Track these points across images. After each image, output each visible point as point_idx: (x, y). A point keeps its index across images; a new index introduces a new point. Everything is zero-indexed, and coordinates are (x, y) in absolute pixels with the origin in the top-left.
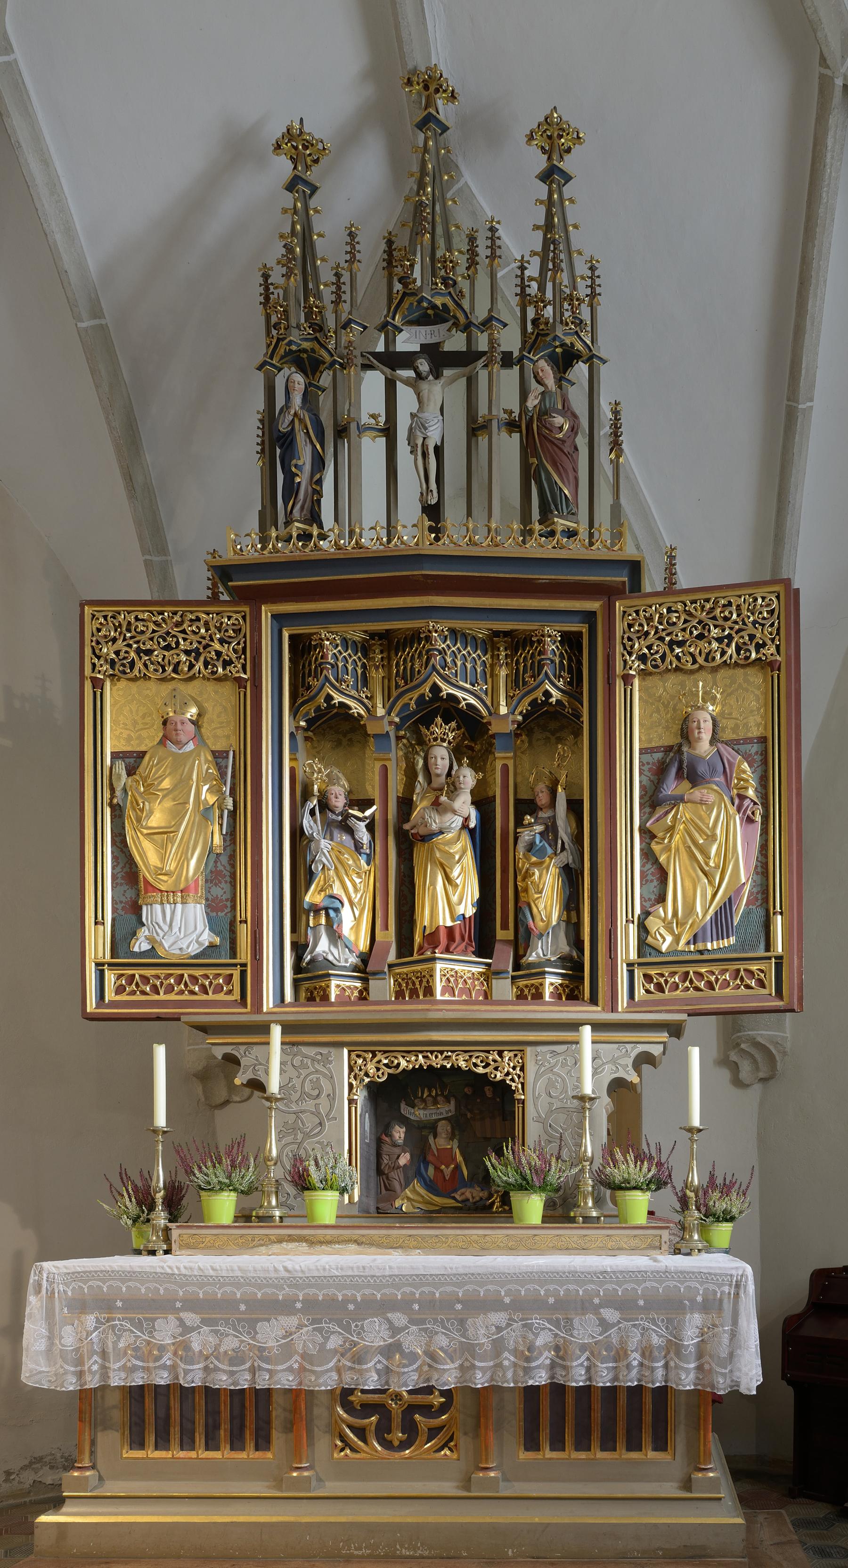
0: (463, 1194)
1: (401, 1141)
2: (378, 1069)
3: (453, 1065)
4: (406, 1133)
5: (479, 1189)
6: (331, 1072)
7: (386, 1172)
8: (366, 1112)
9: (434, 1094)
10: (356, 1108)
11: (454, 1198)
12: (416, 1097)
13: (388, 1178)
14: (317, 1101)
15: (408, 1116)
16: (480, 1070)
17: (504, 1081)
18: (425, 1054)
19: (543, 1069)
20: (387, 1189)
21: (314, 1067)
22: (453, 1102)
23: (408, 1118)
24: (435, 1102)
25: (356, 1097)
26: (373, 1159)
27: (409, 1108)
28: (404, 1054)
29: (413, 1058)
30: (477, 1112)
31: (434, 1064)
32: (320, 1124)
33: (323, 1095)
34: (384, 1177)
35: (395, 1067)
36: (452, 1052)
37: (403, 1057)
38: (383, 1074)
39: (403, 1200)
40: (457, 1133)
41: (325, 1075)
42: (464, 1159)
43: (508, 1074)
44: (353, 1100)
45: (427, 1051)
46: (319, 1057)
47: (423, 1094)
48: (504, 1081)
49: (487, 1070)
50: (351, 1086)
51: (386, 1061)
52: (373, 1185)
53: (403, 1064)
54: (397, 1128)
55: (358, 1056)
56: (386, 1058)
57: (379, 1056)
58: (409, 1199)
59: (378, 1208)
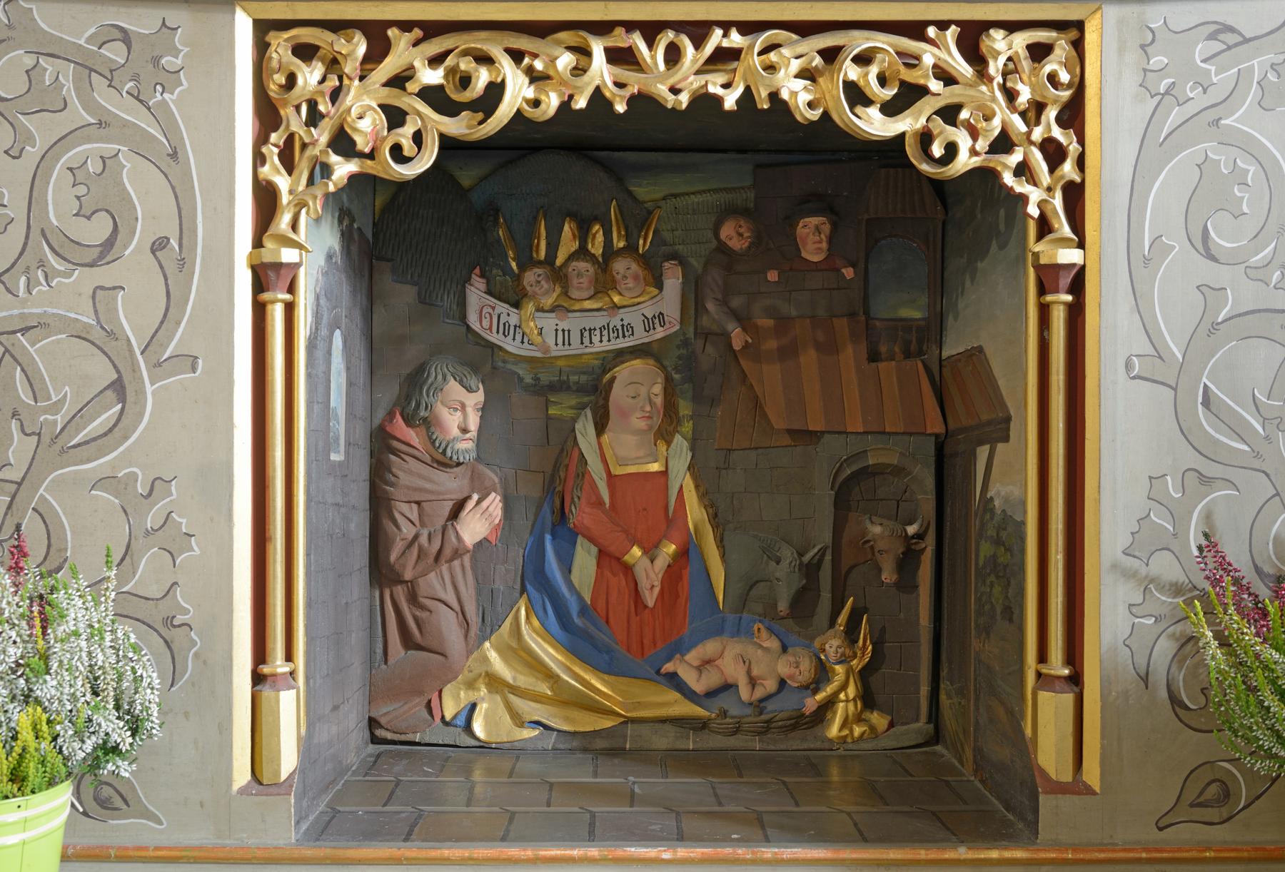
0: (707, 662)
1: (465, 446)
2: (395, 117)
3: (748, 95)
4: (484, 410)
5: (774, 644)
6: (169, 128)
7: (408, 575)
8: (334, 325)
9: (596, 247)
10: (290, 308)
11: (674, 681)
12: (527, 262)
13: (413, 598)
14: (103, 276)
15: (494, 338)
16: (874, 124)
17: (985, 177)
18: (620, 39)
19: (1175, 116)
20: (408, 642)
21: (90, 105)
22: (673, 282)
23: (493, 347)
24: (604, 284)
25: (288, 255)
26: (359, 526)
27: (502, 308)
28: (523, 43)
29: (565, 61)
30: (768, 323)
31: (662, 90)
32: (118, 387)
33: (135, 246)
34: (400, 592)
35: (473, 106)
36: (748, 28)
37: (517, 56)
38: (418, 138)
39: (471, 685)
40: (685, 408)
41: (142, 147)
42: (715, 519)
43: (1003, 143)
44: (278, 266)
45: (630, 26)
46: (116, 53)
47: (553, 247)
48: (985, 177)
49: (907, 124)
50: (266, 199)
51: (433, 77)
52: (356, 637)
53: (518, 90)
54: (454, 389)
55: (305, 52)
56: (435, 61)
57: (402, 52)
58: (495, 683)
59: (373, 723)
